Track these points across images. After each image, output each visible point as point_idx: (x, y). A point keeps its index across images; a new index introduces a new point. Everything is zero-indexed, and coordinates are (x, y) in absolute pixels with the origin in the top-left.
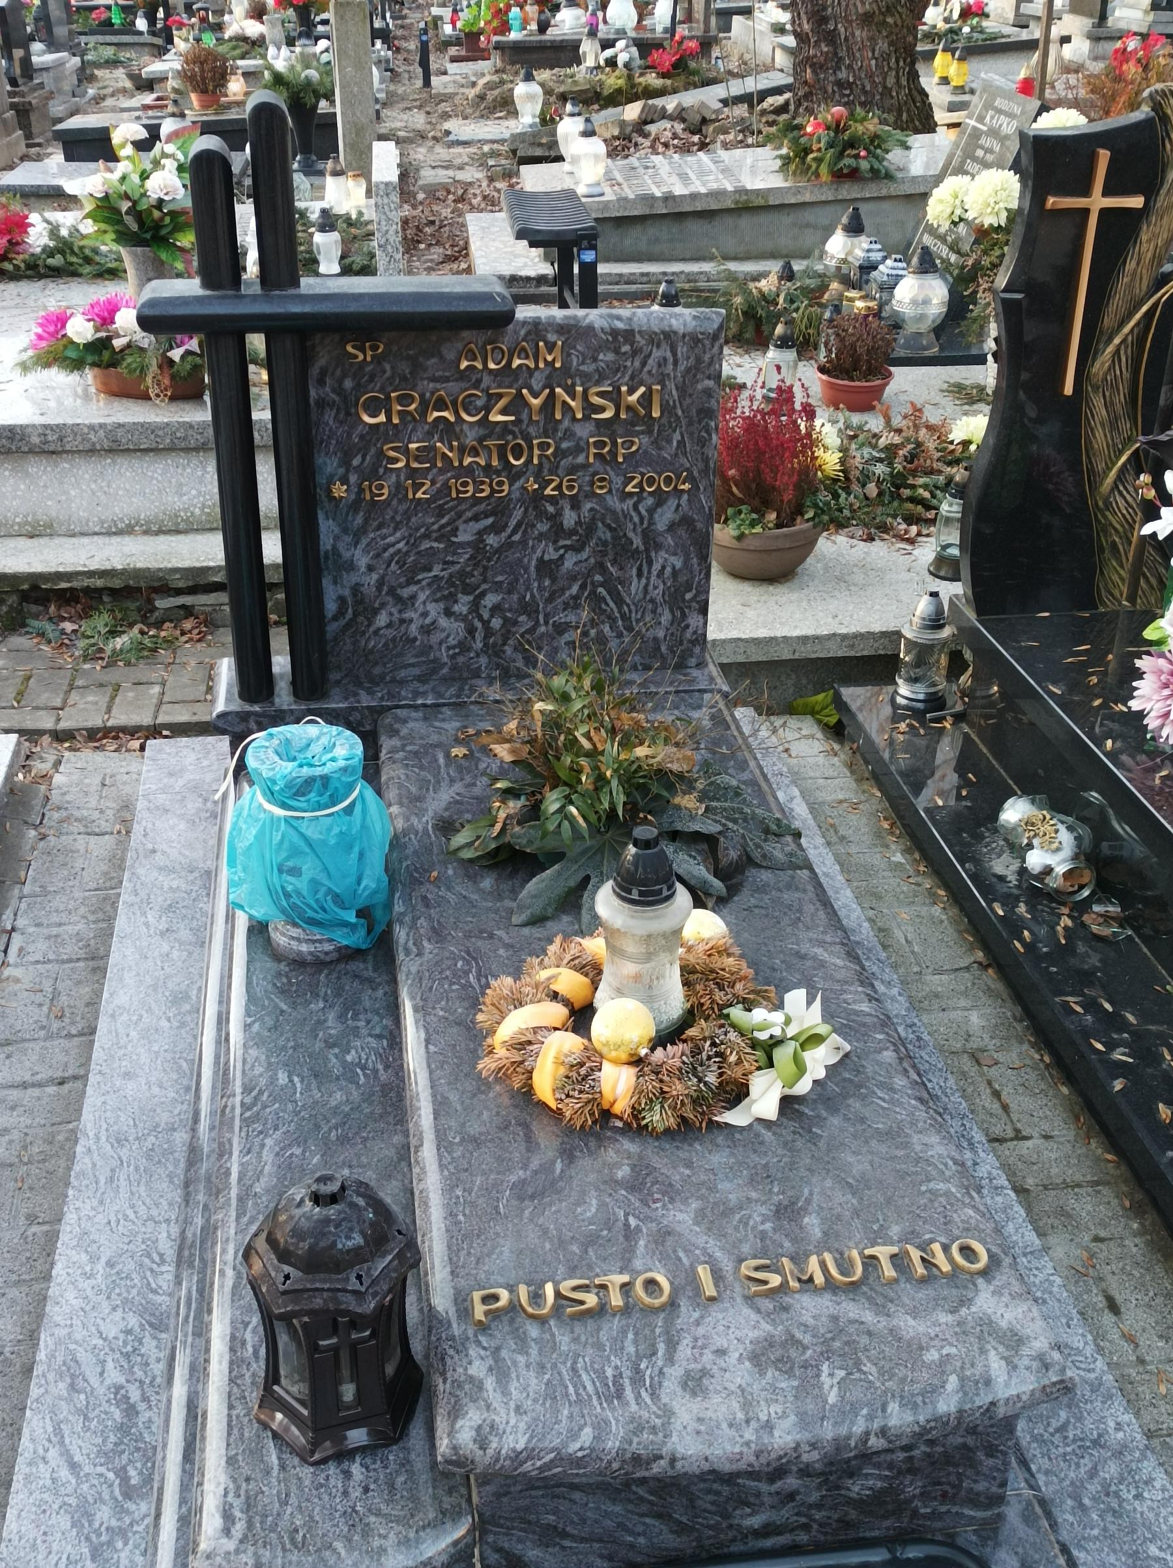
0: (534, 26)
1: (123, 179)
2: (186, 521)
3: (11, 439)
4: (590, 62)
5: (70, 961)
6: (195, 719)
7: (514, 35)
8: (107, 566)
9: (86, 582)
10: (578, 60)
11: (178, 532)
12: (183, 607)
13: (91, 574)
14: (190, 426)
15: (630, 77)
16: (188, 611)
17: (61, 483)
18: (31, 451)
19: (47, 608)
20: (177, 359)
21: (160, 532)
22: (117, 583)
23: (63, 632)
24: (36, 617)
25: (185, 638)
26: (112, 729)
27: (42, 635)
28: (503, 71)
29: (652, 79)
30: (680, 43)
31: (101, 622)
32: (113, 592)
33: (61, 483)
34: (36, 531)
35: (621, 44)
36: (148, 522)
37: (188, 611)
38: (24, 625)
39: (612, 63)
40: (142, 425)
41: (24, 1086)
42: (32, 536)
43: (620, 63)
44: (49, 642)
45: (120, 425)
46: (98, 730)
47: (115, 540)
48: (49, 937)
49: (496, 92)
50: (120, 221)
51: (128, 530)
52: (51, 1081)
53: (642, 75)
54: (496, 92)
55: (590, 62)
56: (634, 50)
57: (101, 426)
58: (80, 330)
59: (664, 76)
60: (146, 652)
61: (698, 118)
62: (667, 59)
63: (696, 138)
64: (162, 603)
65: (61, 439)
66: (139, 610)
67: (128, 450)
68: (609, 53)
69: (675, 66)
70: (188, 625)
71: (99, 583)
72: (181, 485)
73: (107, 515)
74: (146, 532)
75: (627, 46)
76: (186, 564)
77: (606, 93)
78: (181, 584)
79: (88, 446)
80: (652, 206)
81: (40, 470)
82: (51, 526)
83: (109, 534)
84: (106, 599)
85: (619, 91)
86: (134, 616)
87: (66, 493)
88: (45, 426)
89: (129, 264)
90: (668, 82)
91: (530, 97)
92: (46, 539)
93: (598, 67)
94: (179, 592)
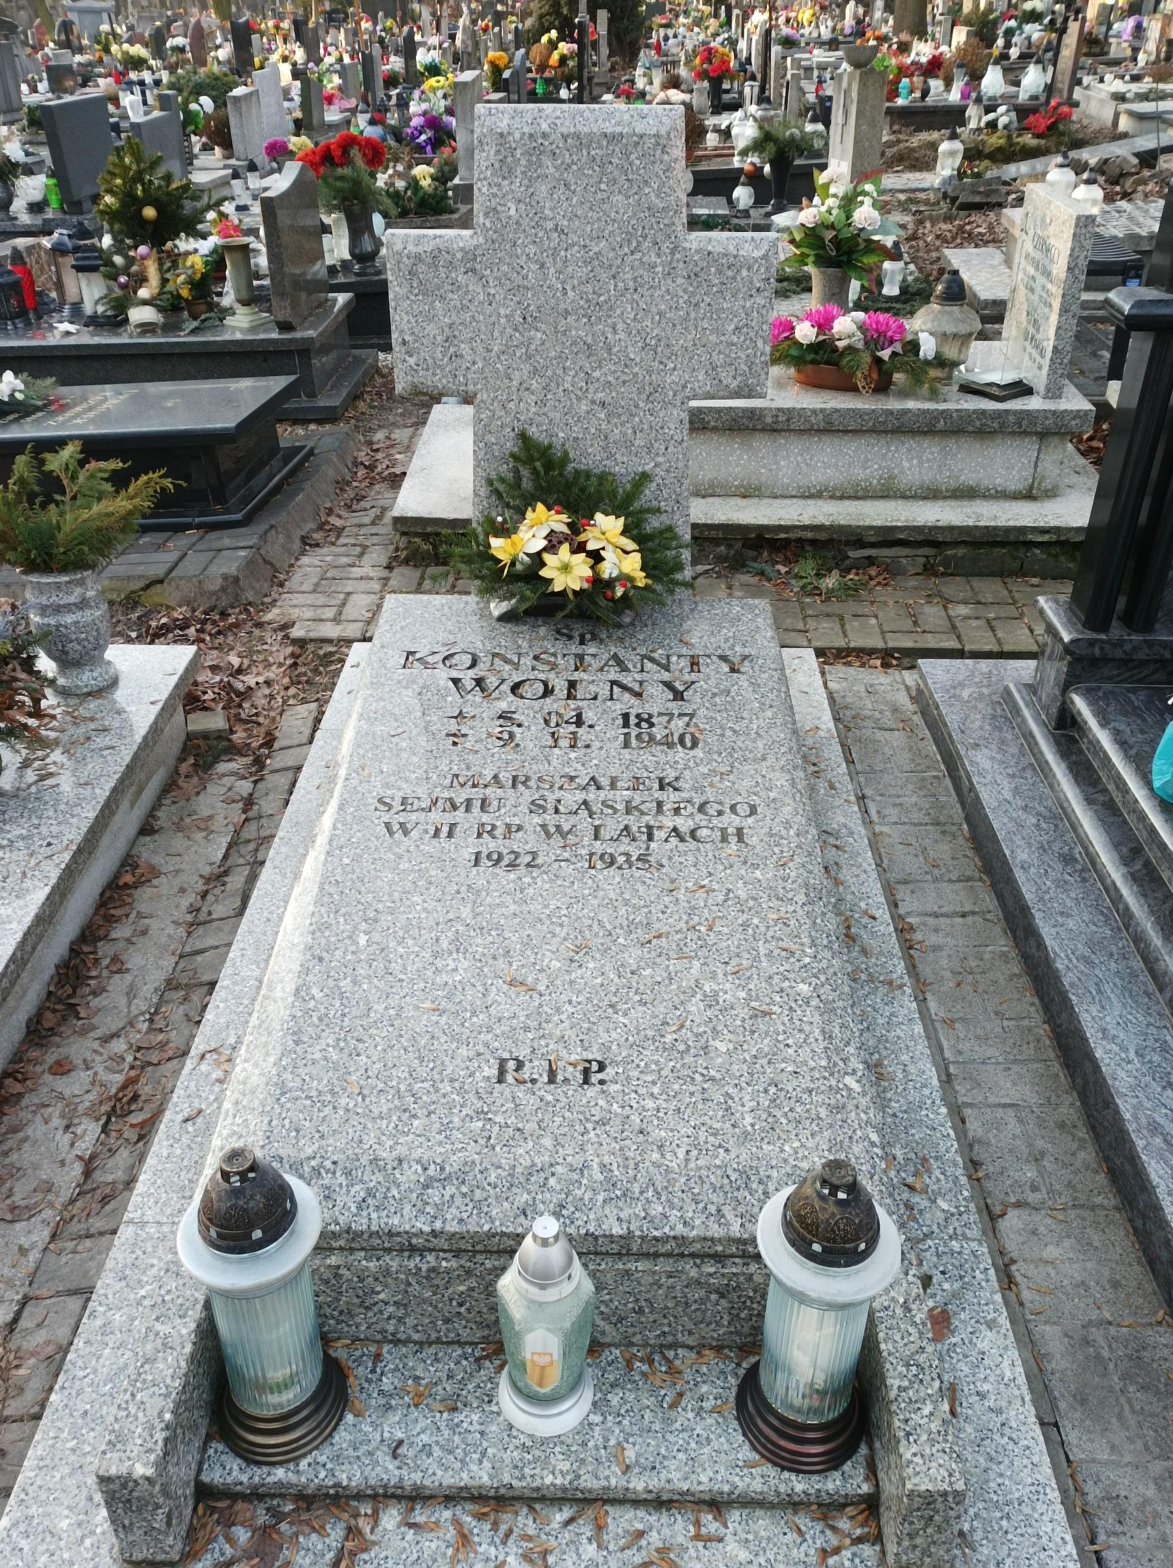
0: (918, 94)
1: (829, 212)
2: (865, 489)
3: (751, 419)
4: (973, 125)
5: (920, 824)
6: (918, 645)
7: (900, 102)
8: (816, 522)
9: (801, 534)
10: (963, 124)
11: (857, 498)
12: (869, 558)
13: (805, 528)
14: (891, 412)
15: (1009, 137)
16: (871, 561)
17: (775, 455)
18: (763, 430)
19: (760, 554)
20: (886, 358)
21: (842, 498)
22: (823, 536)
23: (779, 572)
24: (755, 560)
25: (873, 583)
26: (854, 649)
27: (762, 573)
28: (900, 132)
29: (1028, 139)
30: (1055, 108)
31: (807, 567)
32: (814, 542)
33: (775, 455)
34: (748, 492)
35: (1002, 109)
36: (835, 489)
37: (871, 561)
38: (744, 565)
39: (992, 125)
40: (853, 410)
41: (936, 915)
42: (745, 497)
43: (1000, 125)
44: (769, 580)
45: (837, 410)
46: (843, 649)
47: (811, 502)
48: (895, 805)
49: (895, 149)
50: (823, 247)
51: (818, 495)
52: (955, 914)
53: (1019, 135)
54: (895, 149)
55: (973, 125)
56: (1013, 114)
57: (822, 410)
58: (805, 332)
59: (1038, 136)
60: (850, 592)
61: (1118, 171)
62: (1043, 123)
63: (1118, 188)
64: (854, 554)
65: (788, 420)
66: (834, 558)
67: (838, 431)
68: (991, 116)
69: (1049, 128)
70: (873, 571)
71: (810, 535)
72: (867, 460)
73: (804, 482)
74: (832, 497)
75: (1008, 111)
76: (879, 523)
77: (987, 151)
78: (873, 539)
79: (807, 426)
80: (1138, 244)
81: (762, 444)
82: (759, 489)
83: (804, 497)
84: (808, 548)
85: (1000, 149)
86: (831, 563)
87: (777, 463)
88: (779, 409)
89: (816, 284)
90: (1043, 142)
91: (952, 153)
92: (755, 500)
93: (979, 129)
94: (873, 545)
